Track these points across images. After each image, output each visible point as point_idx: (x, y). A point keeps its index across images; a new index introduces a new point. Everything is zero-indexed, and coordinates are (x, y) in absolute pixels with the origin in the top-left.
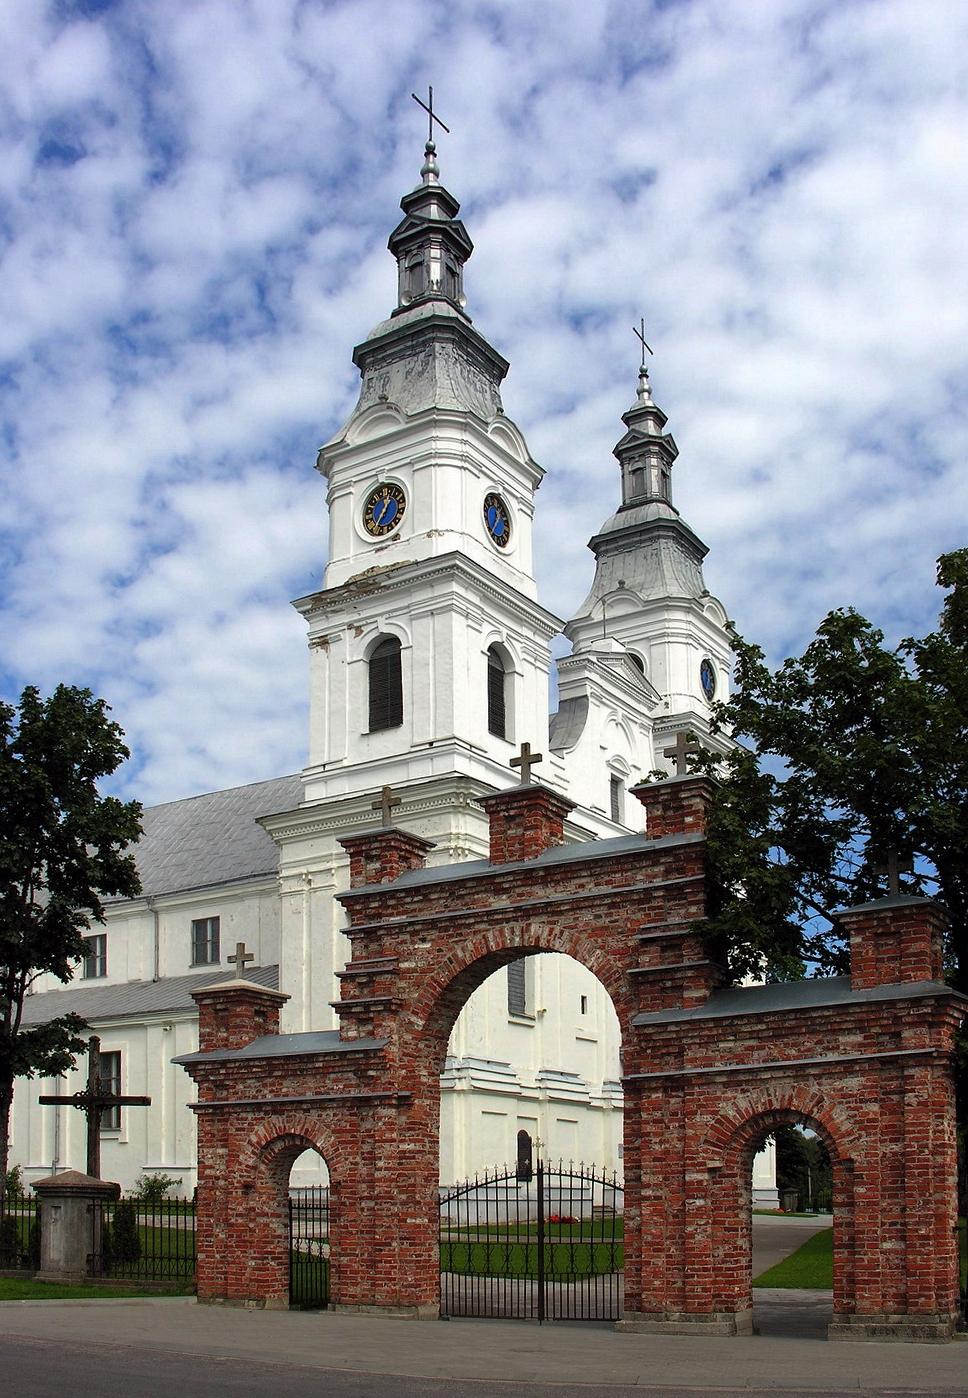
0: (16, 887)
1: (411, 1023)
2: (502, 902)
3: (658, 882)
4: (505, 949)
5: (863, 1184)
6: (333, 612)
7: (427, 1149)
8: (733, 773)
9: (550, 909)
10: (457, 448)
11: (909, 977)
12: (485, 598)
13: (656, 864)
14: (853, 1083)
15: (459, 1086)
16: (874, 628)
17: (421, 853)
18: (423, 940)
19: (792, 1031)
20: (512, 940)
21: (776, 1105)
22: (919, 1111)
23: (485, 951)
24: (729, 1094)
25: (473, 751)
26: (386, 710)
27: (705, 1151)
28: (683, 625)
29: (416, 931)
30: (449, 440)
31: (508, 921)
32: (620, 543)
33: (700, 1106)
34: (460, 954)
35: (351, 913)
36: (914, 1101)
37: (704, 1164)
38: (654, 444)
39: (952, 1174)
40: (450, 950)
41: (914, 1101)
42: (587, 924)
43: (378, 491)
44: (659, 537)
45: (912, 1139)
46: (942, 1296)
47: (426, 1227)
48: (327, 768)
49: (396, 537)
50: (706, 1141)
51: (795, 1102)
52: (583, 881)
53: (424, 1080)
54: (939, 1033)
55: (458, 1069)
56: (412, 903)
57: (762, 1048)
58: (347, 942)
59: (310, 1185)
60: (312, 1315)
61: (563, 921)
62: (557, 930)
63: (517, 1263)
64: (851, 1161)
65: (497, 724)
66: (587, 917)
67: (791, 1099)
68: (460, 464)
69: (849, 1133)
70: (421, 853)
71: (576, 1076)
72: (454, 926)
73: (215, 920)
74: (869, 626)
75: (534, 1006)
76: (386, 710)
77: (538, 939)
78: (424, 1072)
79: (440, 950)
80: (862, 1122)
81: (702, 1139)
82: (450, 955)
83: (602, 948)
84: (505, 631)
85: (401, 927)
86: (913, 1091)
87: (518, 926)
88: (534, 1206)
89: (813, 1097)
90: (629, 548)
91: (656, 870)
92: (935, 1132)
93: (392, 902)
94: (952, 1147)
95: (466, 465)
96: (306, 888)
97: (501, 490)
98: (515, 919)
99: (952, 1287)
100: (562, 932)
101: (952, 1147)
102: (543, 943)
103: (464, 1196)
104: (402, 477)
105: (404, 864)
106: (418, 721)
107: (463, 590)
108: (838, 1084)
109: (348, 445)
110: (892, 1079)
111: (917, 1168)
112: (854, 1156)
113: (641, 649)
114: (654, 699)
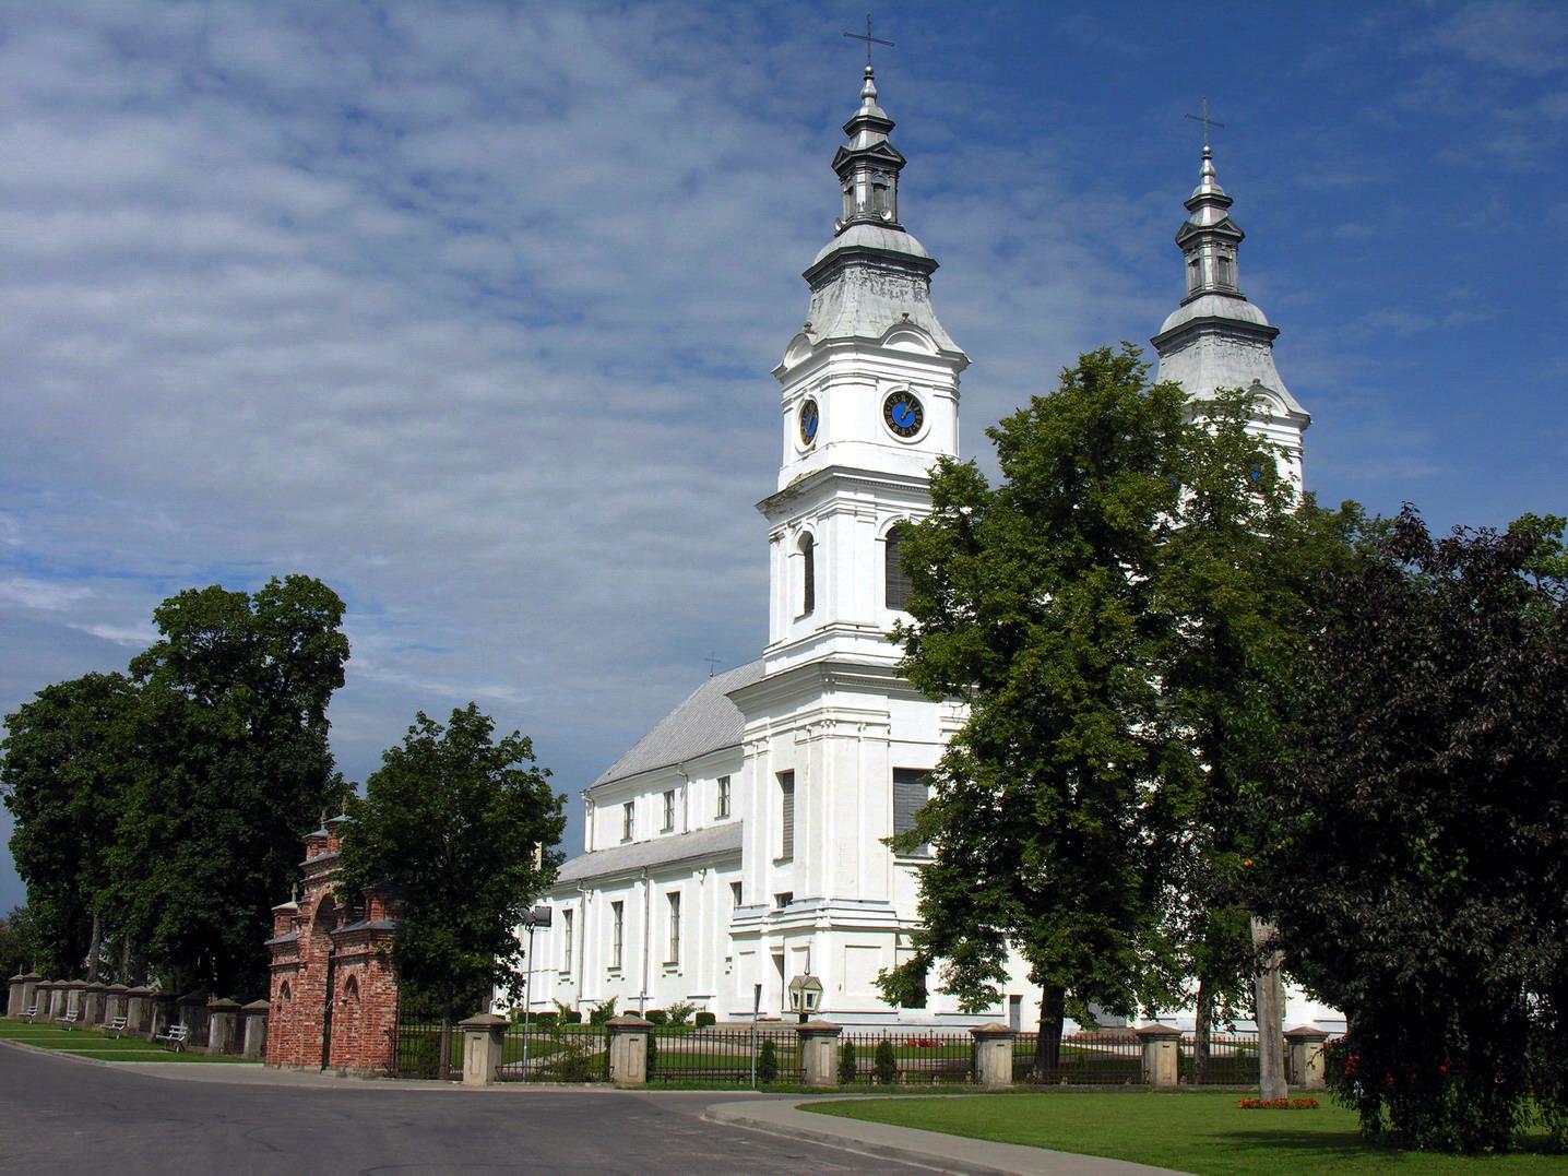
0: (269, 851)
6: (781, 512)
8: (28, 884)
15: (820, 923)
30: (843, 363)
32: (1173, 343)
38: (1207, 234)
44: (1200, 335)
47: (313, 1027)
48: (861, 629)
49: (813, 448)
55: (823, 910)
60: (991, 1166)
71: (887, 903)
104: (817, 393)
107: (852, 493)
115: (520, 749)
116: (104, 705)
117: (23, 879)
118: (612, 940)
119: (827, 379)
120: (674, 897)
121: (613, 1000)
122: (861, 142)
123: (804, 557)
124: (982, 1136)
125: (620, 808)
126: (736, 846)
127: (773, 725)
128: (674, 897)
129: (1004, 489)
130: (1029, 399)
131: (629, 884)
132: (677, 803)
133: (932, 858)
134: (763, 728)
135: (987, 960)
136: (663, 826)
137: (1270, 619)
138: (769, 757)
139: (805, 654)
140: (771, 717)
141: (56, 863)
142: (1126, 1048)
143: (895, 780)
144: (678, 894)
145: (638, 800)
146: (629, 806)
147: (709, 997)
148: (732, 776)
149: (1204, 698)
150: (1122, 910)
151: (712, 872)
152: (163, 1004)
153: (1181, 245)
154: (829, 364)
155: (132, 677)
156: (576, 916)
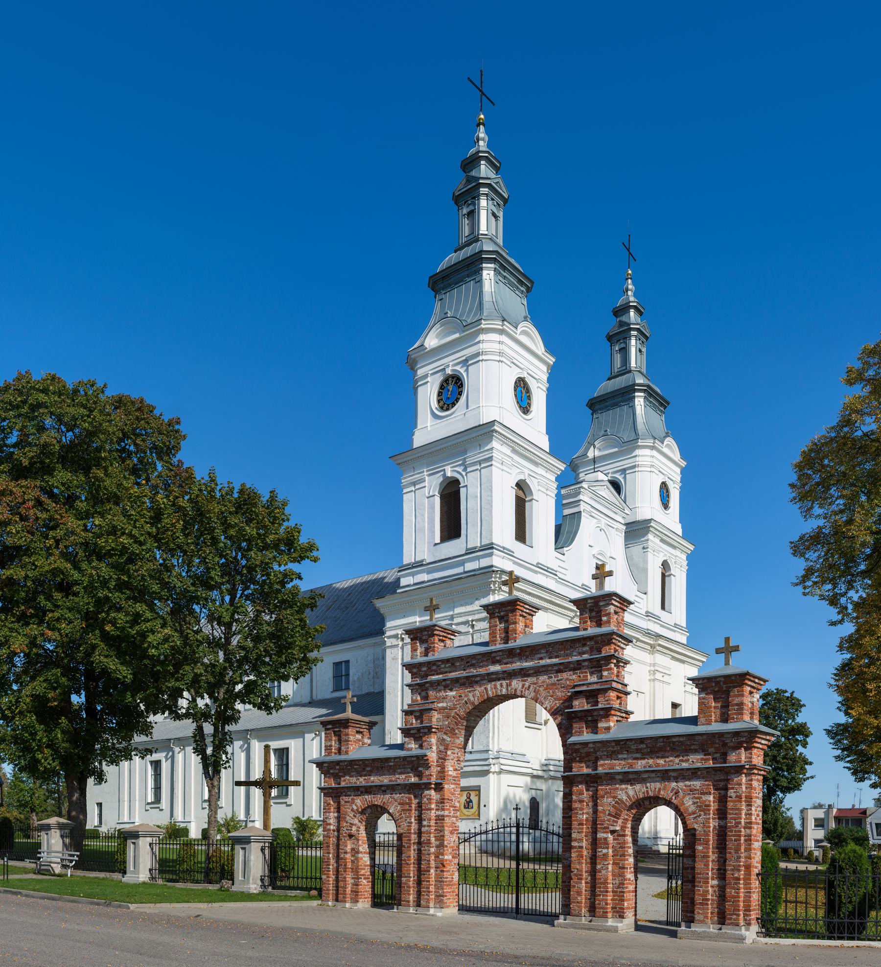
1: (443, 739)
2: (496, 668)
3: (585, 656)
4: (497, 696)
5: (700, 844)
7: (451, 814)
9: (523, 673)
10: (496, 347)
11: (733, 718)
12: (514, 451)
13: (584, 645)
14: (697, 784)
16: (790, 691)
17: (452, 637)
18: (451, 690)
19: (661, 749)
20: (501, 691)
21: (651, 794)
22: (736, 801)
23: (486, 697)
24: (623, 786)
25: (508, 552)
26: (451, 527)
27: (609, 820)
28: (649, 459)
29: (449, 685)
31: (499, 680)
33: (606, 793)
34: (472, 699)
35: (414, 676)
36: (733, 795)
37: (608, 828)
39: (758, 841)
40: (466, 696)
41: (733, 795)
42: (543, 682)
45: (731, 818)
46: (747, 915)
50: (609, 815)
51: (662, 792)
52: (542, 655)
53: (450, 773)
54: (751, 754)
56: (445, 667)
57: (644, 759)
58: (408, 691)
59: (387, 831)
61: (530, 680)
62: (527, 684)
63: (504, 880)
64: (695, 829)
65: (521, 535)
66: (543, 678)
67: (660, 790)
68: (498, 358)
69: (694, 813)
70: (452, 637)
72: (470, 682)
73: (347, 662)
74: (786, 691)
76: (451, 527)
77: (516, 690)
78: (451, 769)
79: (460, 696)
80: (700, 807)
81: (607, 812)
82: (466, 699)
83: (552, 696)
84: (527, 472)
85: (439, 682)
86: (733, 788)
87: (504, 683)
88: (514, 847)
89: (673, 789)
90: (607, 408)
91: (584, 649)
92: (746, 814)
93: (434, 668)
94: (758, 824)
95: (502, 359)
96: (401, 643)
98: (504, 679)
99: (754, 910)
100: (529, 687)
101: (758, 824)
102: (519, 693)
103: (473, 839)
105: (442, 644)
106: (471, 535)
108: (688, 783)
110: (721, 781)
111: (734, 836)
112: (696, 826)
113: (620, 477)
114: (626, 511)
115: (838, 758)
117: (316, 661)
119: (478, 354)
124: (705, 737)
126: (377, 690)
130: (789, 490)
133: (810, 859)
135: (158, 668)
137: (630, 808)
139: (471, 779)
141: (262, 542)
142: (496, 866)
149: (42, 679)
150: (855, 754)
152: (576, 726)
153: (665, 407)
154: (479, 342)
155: (386, 816)
156: (165, 766)
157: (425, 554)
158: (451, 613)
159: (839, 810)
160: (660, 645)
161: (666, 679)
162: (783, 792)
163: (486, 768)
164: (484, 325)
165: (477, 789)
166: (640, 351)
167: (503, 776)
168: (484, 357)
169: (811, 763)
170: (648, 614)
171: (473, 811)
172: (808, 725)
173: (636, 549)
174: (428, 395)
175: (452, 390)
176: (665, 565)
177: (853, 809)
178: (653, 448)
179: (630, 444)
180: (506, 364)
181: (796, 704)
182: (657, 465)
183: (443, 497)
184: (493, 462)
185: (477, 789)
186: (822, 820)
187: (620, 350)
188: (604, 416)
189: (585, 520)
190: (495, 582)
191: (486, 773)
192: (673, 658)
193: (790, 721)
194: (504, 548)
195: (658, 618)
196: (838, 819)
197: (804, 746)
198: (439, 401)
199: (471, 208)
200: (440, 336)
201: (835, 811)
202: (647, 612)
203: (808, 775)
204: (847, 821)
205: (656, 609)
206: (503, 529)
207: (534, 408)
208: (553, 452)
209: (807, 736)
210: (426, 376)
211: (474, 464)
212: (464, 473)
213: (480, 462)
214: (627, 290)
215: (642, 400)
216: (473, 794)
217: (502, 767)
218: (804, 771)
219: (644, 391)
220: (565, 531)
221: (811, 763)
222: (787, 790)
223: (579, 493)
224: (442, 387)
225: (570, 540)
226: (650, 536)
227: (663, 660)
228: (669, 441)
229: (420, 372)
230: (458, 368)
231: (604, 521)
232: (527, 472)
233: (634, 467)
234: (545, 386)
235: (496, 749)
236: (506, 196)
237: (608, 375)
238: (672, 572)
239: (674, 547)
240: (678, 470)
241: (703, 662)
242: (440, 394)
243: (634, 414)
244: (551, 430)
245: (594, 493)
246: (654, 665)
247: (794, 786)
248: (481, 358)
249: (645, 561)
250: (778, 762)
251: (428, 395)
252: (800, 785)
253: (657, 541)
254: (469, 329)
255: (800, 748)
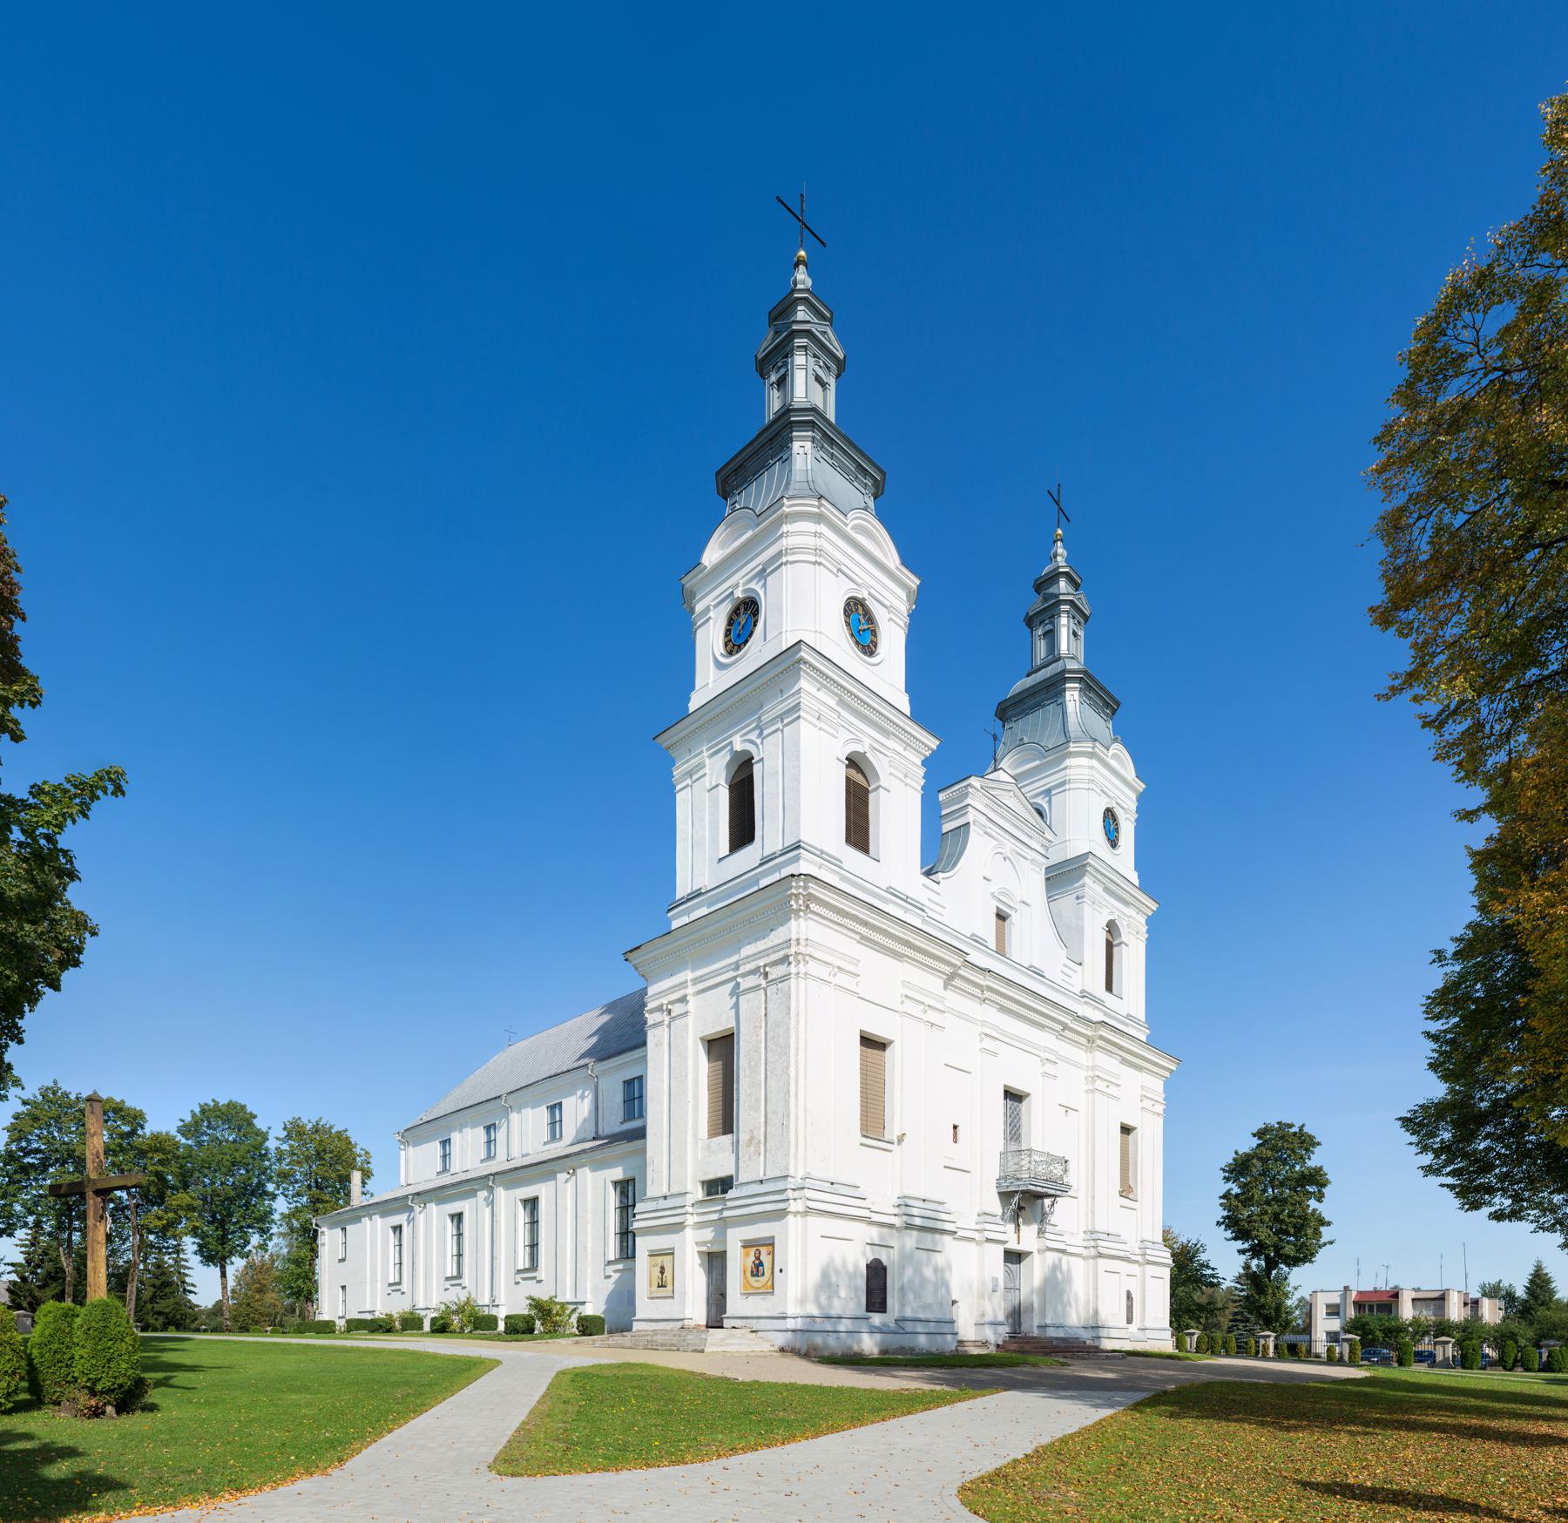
10: (811, 541)
12: (841, 702)
16: (1298, 1125)
25: (835, 862)
26: (743, 830)
28: (1086, 771)
43: (736, 611)
65: (858, 833)
68: (813, 559)
74: (1291, 1126)
75: (896, 1121)
76: (743, 830)
84: (867, 742)
97: (866, 595)
104: (756, 586)
109: (905, 984)
115: (1429, 1170)
116: (1472, 569)
118: (451, 1248)
120: (532, 1204)
121: (107, 1484)
122: (891, 600)
123: (1160, 1121)
125: (436, 1146)
127: (696, 981)
128: (532, 1204)
129: (331, 1227)
131: (472, 1193)
132: (500, 1135)
134: (683, 985)
136: (439, 1169)
138: (690, 1019)
140: (693, 970)
143: (1006, 1261)
144: (400, 1227)
145: (456, 1137)
146: (446, 1143)
147: (1329, 1489)
148: (565, 1102)
151: (377, 1218)
154: (781, 536)
157: (706, 880)
158: (735, 958)
159: (1360, 1293)
160: (1101, 1038)
161: (1112, 1090)
162: (1288, 1265)
163: (781, 1206)
164: (788, 507)
165: (770, 1243)
166: (1075, 634)
167: (812, 1220)
168: (790, 558)
169: (1329, 1224)
170: (1084, 994)
171: (763, 1279)
172: (1325, 1170)
173: (1066, 902)
174: (711, 636)
175: (745, 615)
176: (1112, 928)
177: (1376, 1292)
178: (1092, 755)
179: (1058, 752)
180: (823, 568)
181: (1306, 1142)
182: (1097, 781)
183: (732, 788)
184: (801, 713)
185: (770, 1243)
186: (1338, 1306)
187: (1045, 634)
188: (1020, 726)
189: (975, 835)
190: (797, 896)
191: (781, 1214)
192: (1124, 1061)
193: (1298, 1168)
194: (822, 852)
195: (1101, 1002)
196: (1359, 1305)
197: (1319, 1200)
198: (726, 645)
199: (783, 371)
200: (723, 546)
201: (1354, 1294)
202: (1083, 991)
203: (1322, 1241)
204: (1371, 1308)
205: (1097, 985)
206: (823, 819)
207: (882, 648)
208: (917, 716)
209: (1324, 1185)
210: (707, 610)
211: (772, 721)
212: (758, 741)
213: (781, 717)
214: (1056, 555)
215: (1076, 694)
216: (764, 1250)
217: (810, 1204)
218: (1317, 1234)
219: (1080, 680)
220: (940, 849)
221: (1329, 1224)
222: (1294, 1262)
223: (966, 796)
224: (731, 622)
225: (952, 861)
226: (1087, 880)
227: (1108, 1063)
228: (1118, 748)
229: (699, 608)
230: (752, 585)
231: (1009, 846)
232: (867, 742)
233: (1064, 783)
234: (904, 621)
235: (801, 1174)
236: (840, 355)
237: (1029, 669)
238: (1124, 938)
239: (1127, 903)
240: (1134, 797)
241: (1171, 1071)
242: (728, 632)
243: (1064, 713)
244: (910, 688)
245: (995, 800)
246: (1094, 1068)
247: (1303, 1256)
248: (784, 559)
249: (1080, 917)
250: (1282, 1222)
251: (711, 636)
252: (1312, 1255)
253: (1099, 889)
254: (769, 521)
255: (1313, 1204)
